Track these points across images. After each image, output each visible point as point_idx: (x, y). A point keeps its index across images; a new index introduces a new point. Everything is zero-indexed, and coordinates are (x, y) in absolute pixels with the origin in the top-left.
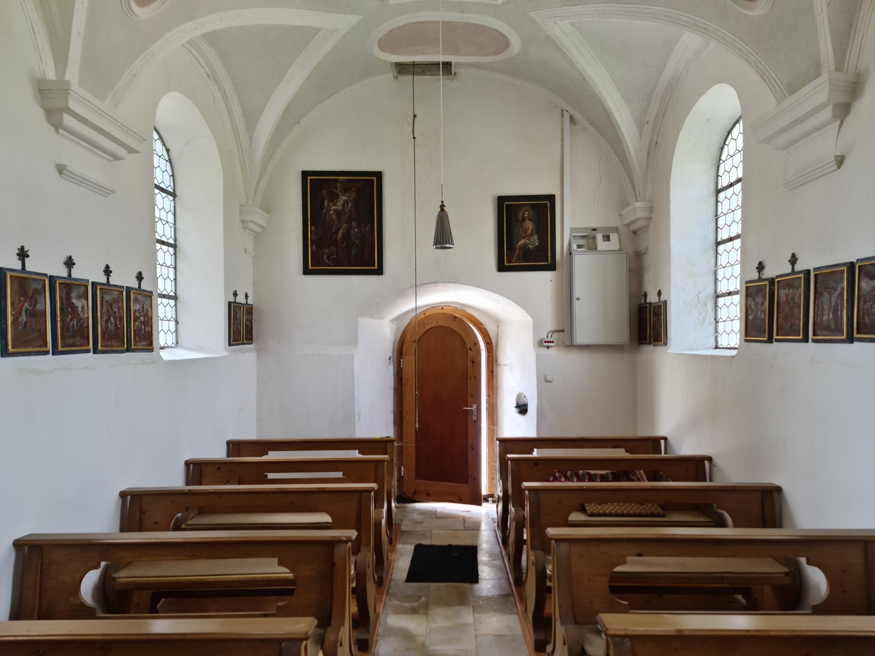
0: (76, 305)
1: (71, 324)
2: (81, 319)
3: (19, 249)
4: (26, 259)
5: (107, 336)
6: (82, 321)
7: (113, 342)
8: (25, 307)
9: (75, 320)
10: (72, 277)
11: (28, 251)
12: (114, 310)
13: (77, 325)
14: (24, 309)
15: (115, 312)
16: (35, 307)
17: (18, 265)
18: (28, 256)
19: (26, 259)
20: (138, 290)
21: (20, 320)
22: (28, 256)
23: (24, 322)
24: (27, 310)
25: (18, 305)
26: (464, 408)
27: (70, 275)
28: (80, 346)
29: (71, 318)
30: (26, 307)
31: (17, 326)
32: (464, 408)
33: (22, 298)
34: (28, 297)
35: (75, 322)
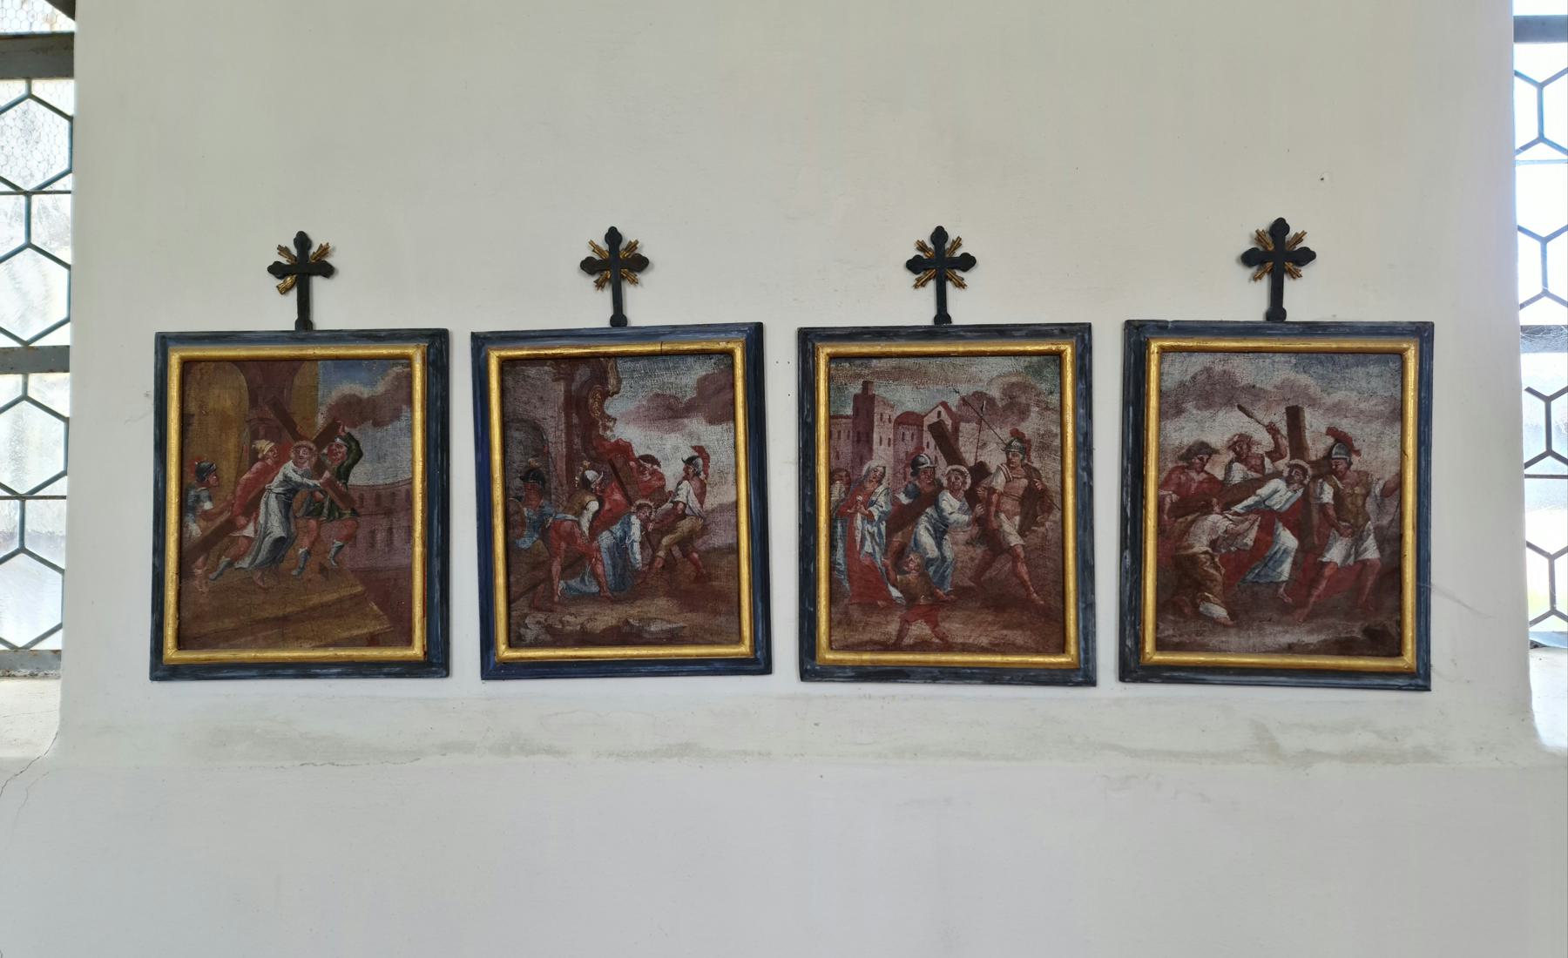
0: (639, 451)
1: (605, 539)
2: (684, 516)
3: (324, 250)
4: (318, 283)
5: (895, 593)
6: (685, 525)
7: (945, 626)
8: (280, 477)
9: (636, 523)
10: (1289, 318)
11: (283, 250)
12: (969, 455)
13: (648, 540)
14: (276, 484)
15: (980, 471)
16: (343, 473)
17: (280, 313)
18: (328, 271)
19: (318, 283)
20: (303, 340)
21: (249, 531)
22: (328, 271)
23: (268, 541)
24: (291, 491)
25: (240, 473)
26: (1206, 594)
27: (619, 319)
28: (673, 638)
29: (596, 514)
30: (287, 479)
31: (225, 560)
32: (1206, 594)
33: (265, 446)
34: (299, 437)
35: (636, 532)
